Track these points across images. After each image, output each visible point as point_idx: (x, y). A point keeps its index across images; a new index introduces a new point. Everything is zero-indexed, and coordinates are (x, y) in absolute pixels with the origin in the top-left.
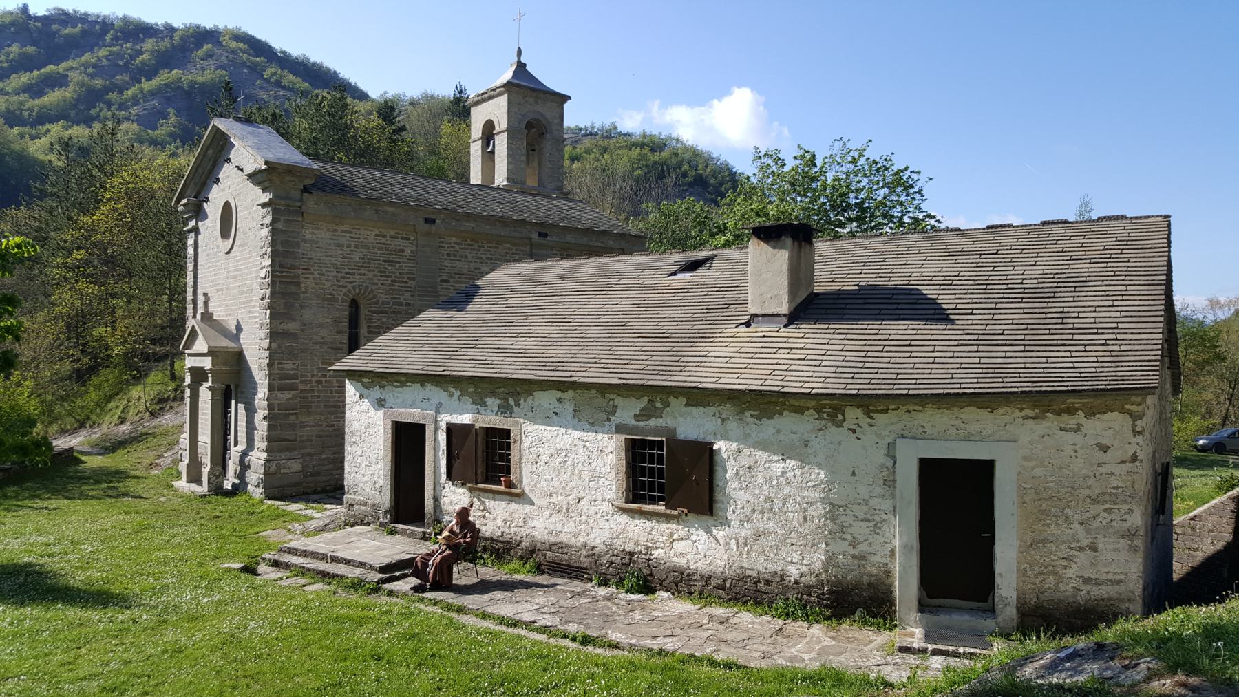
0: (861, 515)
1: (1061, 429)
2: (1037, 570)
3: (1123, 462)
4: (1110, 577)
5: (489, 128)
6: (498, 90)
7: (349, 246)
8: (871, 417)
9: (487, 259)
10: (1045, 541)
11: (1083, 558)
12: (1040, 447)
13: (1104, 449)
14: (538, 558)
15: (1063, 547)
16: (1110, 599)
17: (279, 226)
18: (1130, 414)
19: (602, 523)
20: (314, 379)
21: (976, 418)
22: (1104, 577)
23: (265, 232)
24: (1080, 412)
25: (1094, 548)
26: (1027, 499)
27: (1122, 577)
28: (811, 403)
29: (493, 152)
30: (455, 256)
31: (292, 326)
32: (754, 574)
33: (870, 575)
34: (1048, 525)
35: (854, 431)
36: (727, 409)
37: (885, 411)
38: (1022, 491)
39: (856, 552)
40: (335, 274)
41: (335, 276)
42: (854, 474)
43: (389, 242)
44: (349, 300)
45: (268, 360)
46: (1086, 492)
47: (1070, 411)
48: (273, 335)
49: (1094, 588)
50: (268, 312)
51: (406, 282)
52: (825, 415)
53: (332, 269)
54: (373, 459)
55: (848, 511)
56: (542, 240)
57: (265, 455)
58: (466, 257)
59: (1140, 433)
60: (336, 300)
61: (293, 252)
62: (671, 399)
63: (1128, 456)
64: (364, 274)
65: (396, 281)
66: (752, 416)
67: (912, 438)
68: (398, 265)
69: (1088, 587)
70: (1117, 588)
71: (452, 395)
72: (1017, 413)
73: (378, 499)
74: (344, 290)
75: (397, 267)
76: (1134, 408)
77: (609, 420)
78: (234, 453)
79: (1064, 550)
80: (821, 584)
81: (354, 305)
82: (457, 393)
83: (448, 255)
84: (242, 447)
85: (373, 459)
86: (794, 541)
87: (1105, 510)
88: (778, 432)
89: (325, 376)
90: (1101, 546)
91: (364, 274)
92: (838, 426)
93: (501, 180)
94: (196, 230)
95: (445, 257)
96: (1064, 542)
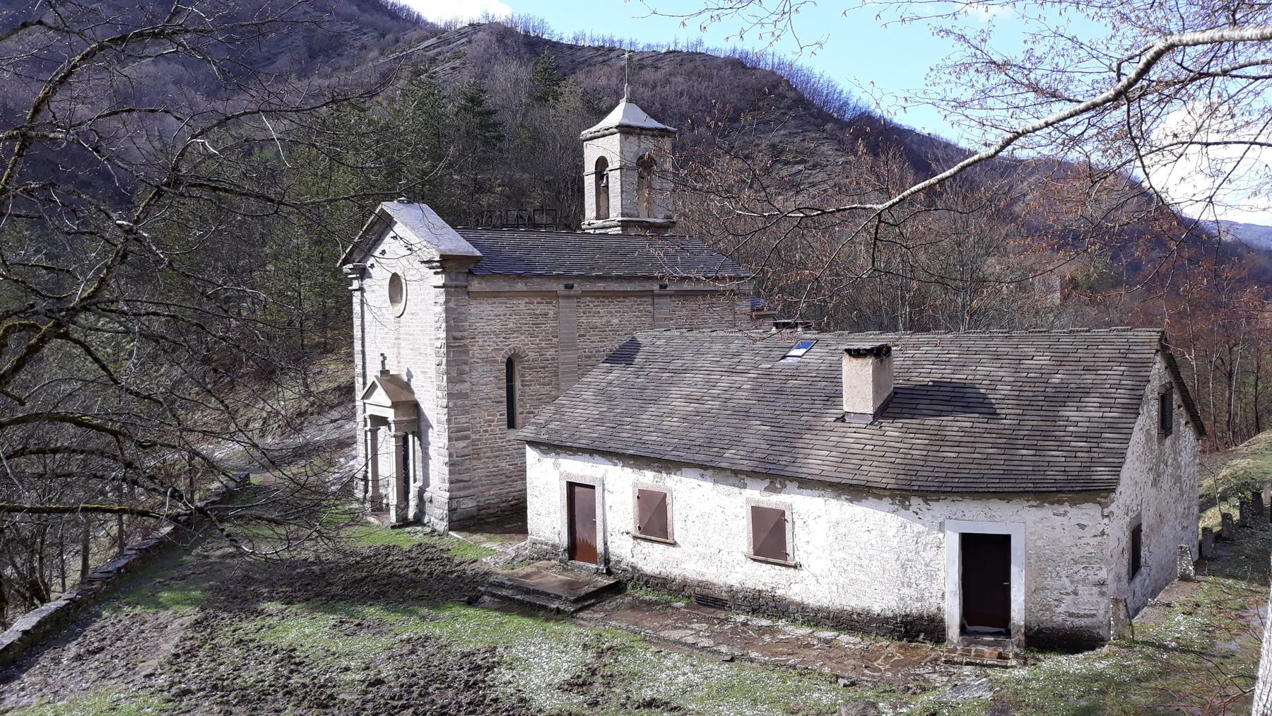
1: (1054, 514)
2: (1038, 608)
3: (1095, 536)
4: (1087, 612)
5: (602, 163)
6: (611, 130)
7: (505, 315)
8: (928, 504)
10: (1044, 588)
11: (1068, 600)
12: (1041, 526)
14: (688, 592)
16: (1086, 627)
17: (452, 305)
18: (1100, 503)
19: (738, 568)
22: (1082, 612)
23: (440, 309)
24: (1067, 503)
25: (1076, 594)
26: (1032, 561)
27: (1095, 612)
28: (887, 493)
29: (607, 187)
30: (590, 312)
31: (465, 387)
32: (849, 609)
34: (1046, 578)
35: (917, 514)
37: (938, 500)
38: (1028, 558)
40: (495, 339)
41: (494, 342)
43: (536, 307)
44: (505, 360)
45: (446, 417)
46: (1071, 556)
48: (450, 396)
49: (1076, 620)
50: (445, 377)
51: (551, 340)
52: (897, 502)
54: (552, 509)
56: (663, 292)
57: (448, 494)
58: (599, 312)
59: (1107, 516)
60: (496, 361)
61: (462, 326)
62: (787, 482)
63: (1098, 533)
64: (517, 337)
65: (543, 340)
67: (955, 519)
68: (543, 326)
69: (1072, 619)
72: (1026, 504)
73: (557, 541)
74: (503, 352)
75: (544, 328)
76: (1103, 500)
78: (414, 488)
79: (1056, 595)
80: (895, 617)
81: (510, 363)
83: (584, 313)
84: (419, 484)
85: (552, 509)
86: (877, 587)
87: (1083, 568)
90: (1080, 592)
91: (517, 337)
92: (906, 509)
93: (615, 214)
94: (361, 289)
95: (582, 315)
96: (1056, 589)
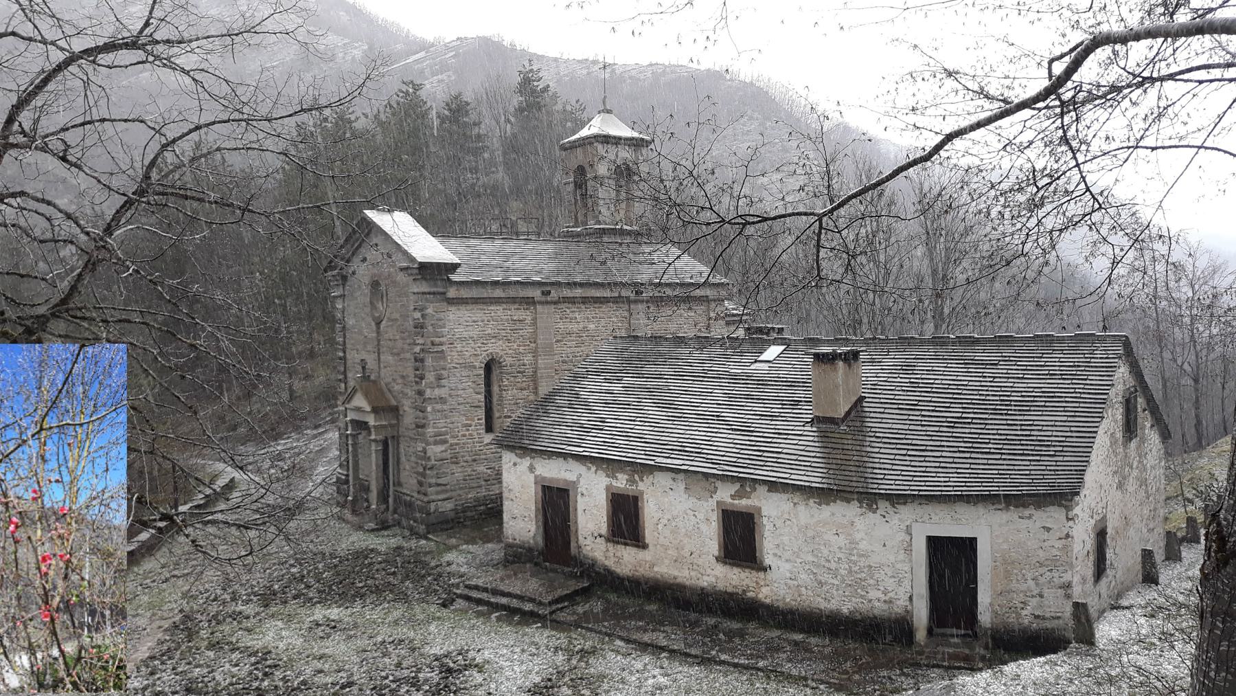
0: (890, 574)
1: (1020, 517)
3: (1060, 539)
4: (1053, 614)
9: (593, 318)
11: (1034, 602)
13: (1048, 529)
15: (1021, 595)
20: (460, 434)
21: (963, 510)
25: (1041, 596)
33: (896, 614)
36: (797, 497)
39: (887, 598)
42: (884, 545)
44: (483, 365)
47: (1025, 506)
53: (471, 342)
55: (881, 571)
58: (576, 318)
59: (1071, 519)
63: (1063, 535)
65: (520, 346)
66: (815, 502)
68: (521, 331)
70: (1056, 621)
71: (589, 469)
77: (712, 497)
79: (1022, 597)
81: (488, 368)
82: (594, 469)
88: (833, 514)
89: (468, 430)
92: (873, 513)
